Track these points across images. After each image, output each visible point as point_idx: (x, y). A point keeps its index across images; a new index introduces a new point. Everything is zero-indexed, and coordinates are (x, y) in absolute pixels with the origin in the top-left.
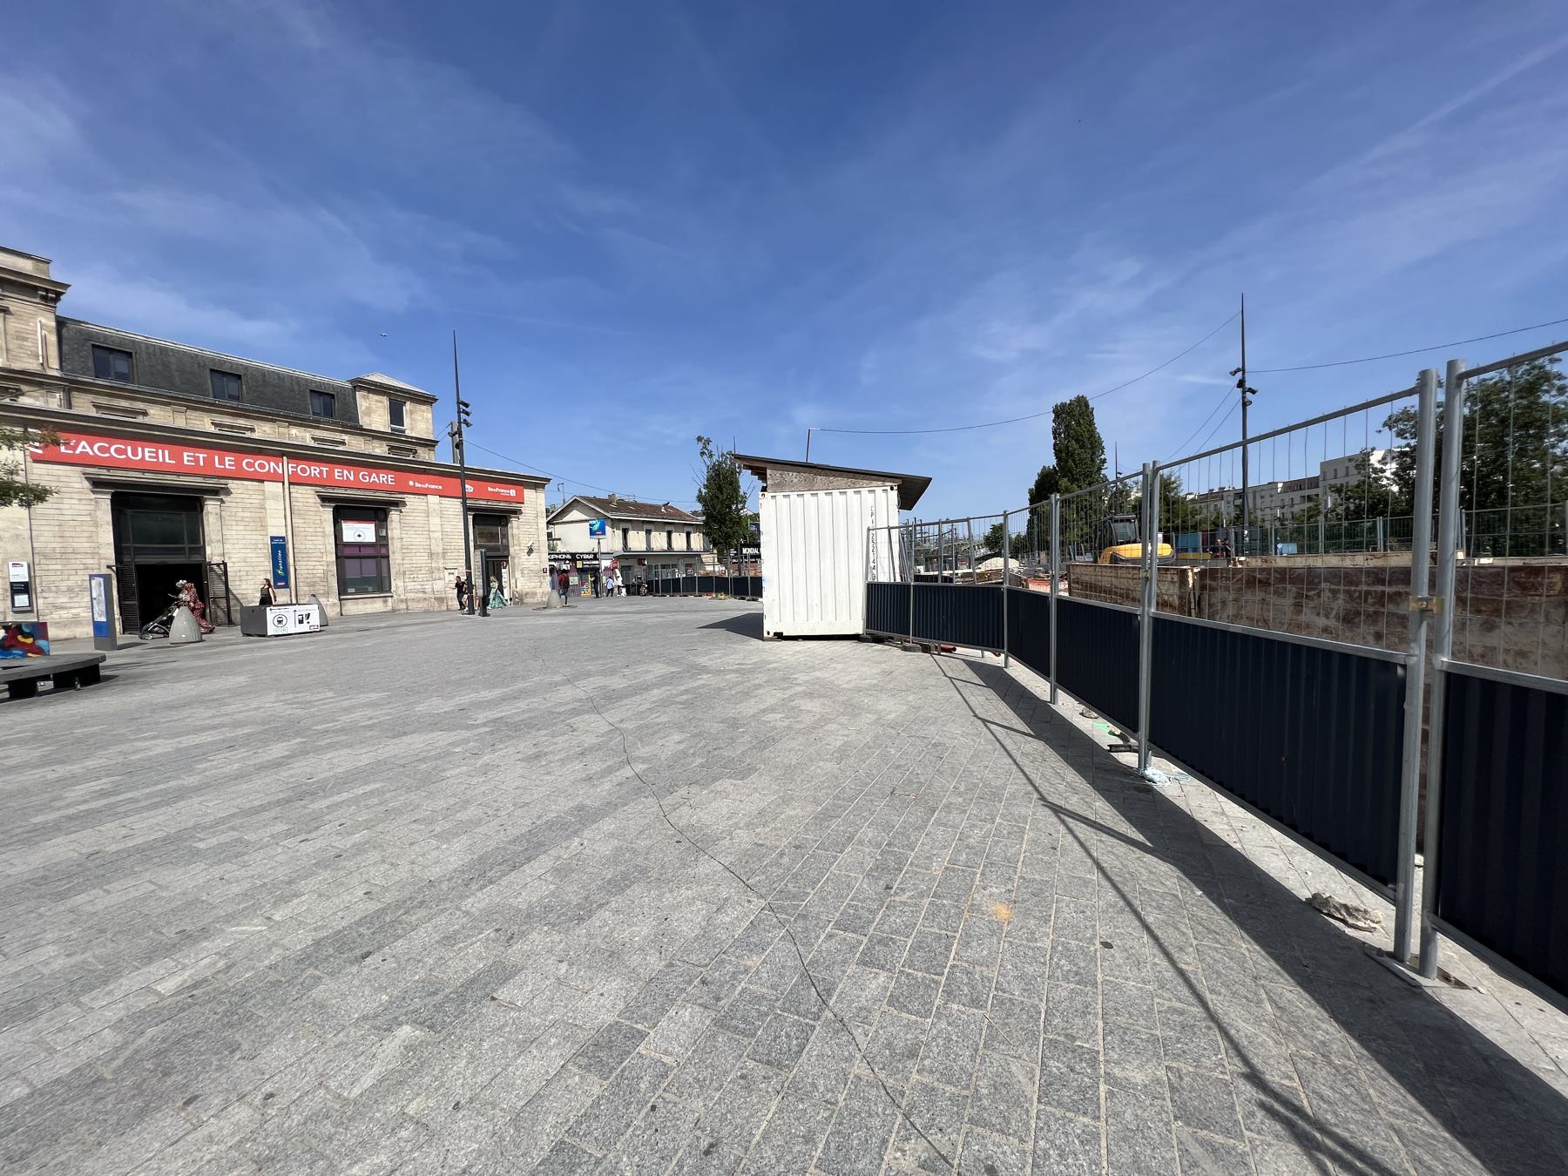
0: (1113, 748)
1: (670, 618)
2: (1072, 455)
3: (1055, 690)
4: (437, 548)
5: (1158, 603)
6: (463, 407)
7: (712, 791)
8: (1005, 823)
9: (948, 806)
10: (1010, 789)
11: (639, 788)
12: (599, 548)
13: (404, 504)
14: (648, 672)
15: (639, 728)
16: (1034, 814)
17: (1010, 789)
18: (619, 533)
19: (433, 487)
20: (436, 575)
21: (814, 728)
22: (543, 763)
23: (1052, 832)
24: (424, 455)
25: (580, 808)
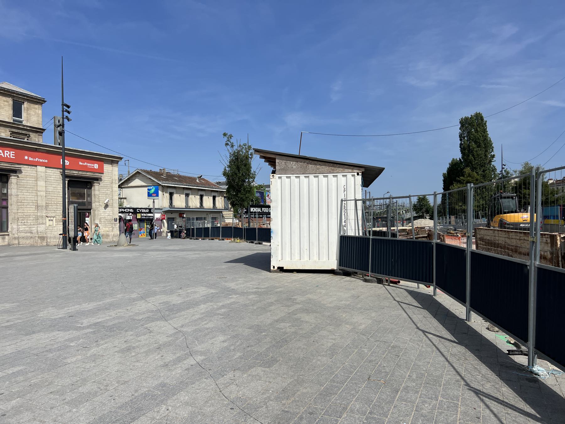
0: (510, 352)
1: (204, 255)
2: (472, 152)
3: (469, 312)
4: (42, 203)
5: (540, 258)
6: (66, 107)
7: (250, 375)
8: (444, 400)
9: (406, 388)
10: (445, 378)
11: (201, 372)
12: (154, 205)
13: (20, 172)
14: (195, 292)
15: (195, 331)
16: (463, 395)
17: (445, 378)
18: (167, 195)
19: (41, 160)
20: (40, 221)
21: (312, 334)
22: (133, 354)
23: (476, 406)
24: (35, 138)
25: (163, 385)
